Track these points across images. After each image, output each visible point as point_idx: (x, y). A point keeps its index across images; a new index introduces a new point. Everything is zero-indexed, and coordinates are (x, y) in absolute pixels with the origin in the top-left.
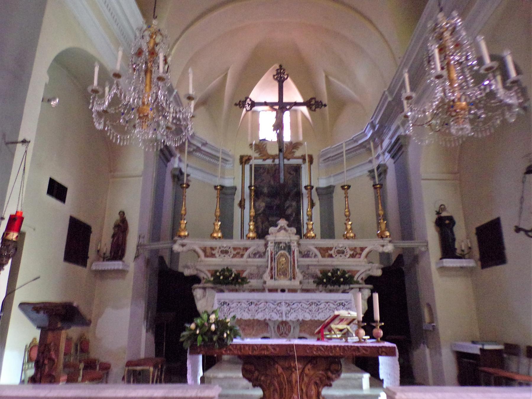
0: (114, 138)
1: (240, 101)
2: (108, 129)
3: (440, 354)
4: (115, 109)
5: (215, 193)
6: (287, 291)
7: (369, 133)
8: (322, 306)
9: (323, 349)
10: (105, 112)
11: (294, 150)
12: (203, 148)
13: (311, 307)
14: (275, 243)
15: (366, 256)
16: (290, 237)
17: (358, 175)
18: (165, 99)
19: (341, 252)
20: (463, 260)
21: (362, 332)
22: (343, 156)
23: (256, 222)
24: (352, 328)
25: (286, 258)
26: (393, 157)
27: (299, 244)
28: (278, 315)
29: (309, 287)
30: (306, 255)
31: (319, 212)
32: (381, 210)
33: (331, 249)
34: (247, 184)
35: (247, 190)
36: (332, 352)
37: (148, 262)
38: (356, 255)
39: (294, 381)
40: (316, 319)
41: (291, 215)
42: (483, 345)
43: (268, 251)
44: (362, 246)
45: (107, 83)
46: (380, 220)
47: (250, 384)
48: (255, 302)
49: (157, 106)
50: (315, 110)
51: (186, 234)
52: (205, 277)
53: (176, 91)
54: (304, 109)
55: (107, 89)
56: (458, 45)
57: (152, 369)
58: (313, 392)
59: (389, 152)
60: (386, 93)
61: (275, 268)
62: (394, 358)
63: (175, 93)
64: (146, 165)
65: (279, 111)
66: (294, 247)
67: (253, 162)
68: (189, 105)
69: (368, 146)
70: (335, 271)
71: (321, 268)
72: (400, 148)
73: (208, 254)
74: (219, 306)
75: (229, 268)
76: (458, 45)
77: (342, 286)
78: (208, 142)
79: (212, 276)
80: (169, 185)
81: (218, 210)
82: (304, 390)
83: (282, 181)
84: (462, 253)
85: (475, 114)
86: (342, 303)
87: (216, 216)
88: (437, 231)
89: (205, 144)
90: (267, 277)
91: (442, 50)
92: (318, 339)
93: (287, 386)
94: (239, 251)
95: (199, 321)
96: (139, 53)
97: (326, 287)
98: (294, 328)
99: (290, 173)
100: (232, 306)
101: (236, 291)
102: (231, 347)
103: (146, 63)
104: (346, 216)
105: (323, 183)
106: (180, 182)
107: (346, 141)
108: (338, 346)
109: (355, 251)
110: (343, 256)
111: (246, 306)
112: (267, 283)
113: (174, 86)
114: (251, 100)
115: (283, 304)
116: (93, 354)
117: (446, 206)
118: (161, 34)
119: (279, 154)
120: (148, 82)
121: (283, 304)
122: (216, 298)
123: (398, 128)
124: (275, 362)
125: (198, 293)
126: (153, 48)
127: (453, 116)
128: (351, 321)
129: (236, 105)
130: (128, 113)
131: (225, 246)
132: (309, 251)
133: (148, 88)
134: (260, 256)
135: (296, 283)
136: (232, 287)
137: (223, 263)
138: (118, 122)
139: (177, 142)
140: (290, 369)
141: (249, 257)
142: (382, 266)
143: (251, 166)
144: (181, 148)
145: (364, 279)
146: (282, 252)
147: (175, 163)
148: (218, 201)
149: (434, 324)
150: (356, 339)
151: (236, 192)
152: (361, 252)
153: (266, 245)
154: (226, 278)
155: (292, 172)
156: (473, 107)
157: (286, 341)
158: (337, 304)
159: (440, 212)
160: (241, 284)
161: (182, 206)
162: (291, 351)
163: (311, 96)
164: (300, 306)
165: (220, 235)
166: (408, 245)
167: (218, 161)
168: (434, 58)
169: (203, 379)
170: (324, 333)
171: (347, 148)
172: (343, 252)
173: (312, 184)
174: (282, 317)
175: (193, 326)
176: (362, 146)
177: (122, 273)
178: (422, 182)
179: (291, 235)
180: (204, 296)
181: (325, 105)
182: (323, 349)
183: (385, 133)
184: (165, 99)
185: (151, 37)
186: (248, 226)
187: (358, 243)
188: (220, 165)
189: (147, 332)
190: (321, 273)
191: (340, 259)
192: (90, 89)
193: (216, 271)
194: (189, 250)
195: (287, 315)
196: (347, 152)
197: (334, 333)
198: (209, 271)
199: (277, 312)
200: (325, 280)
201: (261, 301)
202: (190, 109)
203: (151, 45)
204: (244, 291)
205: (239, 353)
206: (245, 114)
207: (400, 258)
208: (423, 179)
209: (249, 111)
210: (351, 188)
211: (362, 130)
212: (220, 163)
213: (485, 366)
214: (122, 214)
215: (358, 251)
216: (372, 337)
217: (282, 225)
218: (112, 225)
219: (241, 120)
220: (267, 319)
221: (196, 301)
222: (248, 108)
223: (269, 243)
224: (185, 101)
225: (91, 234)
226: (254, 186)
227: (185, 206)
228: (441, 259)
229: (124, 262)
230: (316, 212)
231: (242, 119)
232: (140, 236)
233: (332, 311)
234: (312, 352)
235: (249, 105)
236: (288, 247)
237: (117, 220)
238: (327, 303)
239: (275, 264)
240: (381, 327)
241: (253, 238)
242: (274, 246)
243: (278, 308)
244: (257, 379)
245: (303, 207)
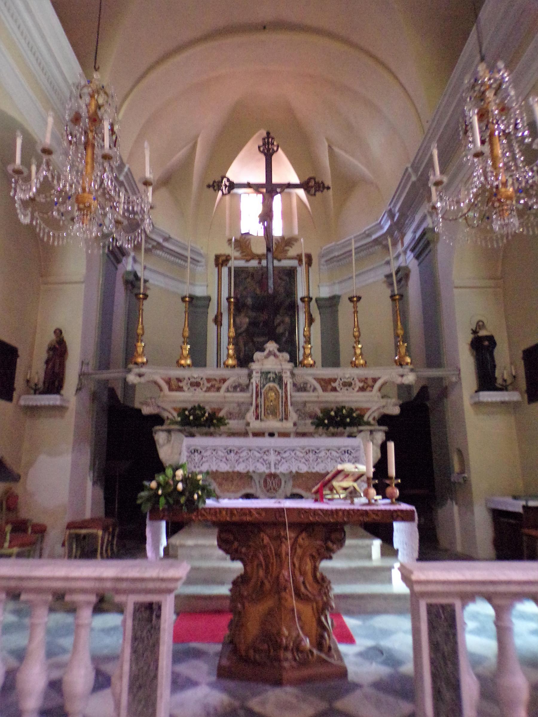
0: (46, 235)
1: (214, 182)
2: (37, 223)
3: (473, 514)
4: (46, 197)
5: (182, 307)
6: (276, 435)
7: (386, 224)
8: (322, 454)
9: (321, 514)
10: (32, 200)
11: (287, 248)
12: (166, 244)
13: (307, 456)
14: (262, 373)
15: (380, 390)
16: (281, 365)
17: (371, 281)
18: (113, 184)
19: (348, 384)
20: (505, 393)
21: (373, 491)
22: (351, 255)
23: (236, 344)
24: (360, 486)
25: (277, 393)
26: (417, 257)
27: (293, 375)
28: (265, 466)
29: (306, 430)
30: (301, 388)
32: (401, 329)
33: (335, 380)
34: (225, 294)
35: (225, 303)
36: (333, 518)
37: (94, 397)
38: (367, 387)
39: (284, 554)
40: (314, 471)
41: (283, 334)
42: (527, 501)
43: (252, 383)
44: (374, 376)
45: (34, 160)
46: (399, 341)
47: (228, 557)
48: (236, 450)
49: (104, 194)
50: (315, 195)
51: (145, 360)
52: (170, 417)
53: (127, 166)
54: (301, 192)
55: (34, 168)
56: (504, 109)
57: (100, 533)
58: (308, 567)
59: (412, 250)
61: (261, 405)
62: (412, 523)
63: (126, 170)
64: (89, 268)
65: (267, 196)
66: (287, 379)
67: (233, 263)
68: (146, 192)
69: (384, 243)
70: (339, 410)
71: (322, 405)
72: (428, 243)
73: (174, 387)
74: (188, 455)
75: (201, 405)
76: (504, 109)
77: (348, 429)
78: (172, 236)
79: (179, 415)
80: (120, 287)
81: (187, 329)
82: (297, 565)
83: (271, 291)
84: (504, 383)
85: (526, 203)
86: (348, 451)
87: (184, 337)
88: (472, 355)
89: (167, 239)
90: (251, 418)
91: (483, 115)
92: (316, 500)
93: (275, 559)
94: (214, 382)
95: (161, 478)
96: (76, 119)
97: (327, 429)
98: (285, 482)
99: (281, 279)
100: (205, 455)
101: (211, 434)
102: (203, 512)
103: (86, 133)
104: (354, 337)
105: (325, 292)
106: (136, 291)
107: (355, 235)
108: (340, 510)
109: (365, 382)
110: (350, 389)
111: (223, 455)
112: (251, 425)
113: (125, 160)
114: (228, 180)
115: (272, 452)
116: (24, 514)
117: (485, 322)
118: (105, 93)
119: (267, 254)
120: (89, 160)
121: (272, 452)
122: (184, 444)
123: (424, 218)
124: (260, 530)
125: (160, 437)
126: (96, 113)
127: (495, 208)
128: (358, 477)
129: (209, 186)
130: (64, 202)
131: (195, 376)
132: (306, 384)
133: (89, 167)
134: (242, 390)
135: (288, 425)
136: (205, 430)
137: (192, 399)
138: (50, 214)
139: (130, 242)
140: (279, 539)
141: (228, 390)
142: (401, 402)
143: (230, 269)
144: (137, 248)
146: (271, 384)
147: (128, 265)
148: (187, 317)
149: (466, 475)
150: (364, 500)
151: (211, 303)
152: (372, 384)
153: (250, 376)
154: (197, 418)
156: (523, 195)
157: (275, 503)
158: (341, 452)
159: (478, 330)
160: (217, 426)
161: (139, 323)
162: (280, 517)
163: (312, 175)
164: (293, 454)
165: (189, 362)
167: (186, 261)
168: (472, 128)
169: (166, 550)
170: (324, 492)
171: (359, 244)
172: (350, 384)
173: (311, 295)
174: (270, 468)
175: (153, 484)
176: (376, 241)
177: (61, 409)
178: (455, 291)
179: (283, 363)
180: (169, 441)
181: (328, 188)
182: (321, 514)
183: (407, 224)
184: (113, 184)
185: (92, 96)
186: (226, 350)
187: (369, 373)
188: (189, 267)
189: (93, 485)
190: (322, 412)
192: (10, 168)
193: (185, 409)
194: (148, 382)
195: (277, 466)
196: (356, 250)
197: (337, 492)
198: (175, 409)
199: (263, 462)
200: (326, 421)
201: (244, 448)
202: (148, 198)
203: (93, 107)
204: (220, 435)
205: (214, 519)
206: (221, 199)
207: (424, 390)
208: (456, 287)
209: (226, 194)
210: (362, 300)
211: (377, 220)
212: (189, 264)
213: (528, 528)
214: (59, 332)
215: (370, 382)
216: (384, 497)
217: (271, 349)
218: (45, 347)
220: (251, 470)
221: (158, 447)
222: (225, 191)
223: (254, 373)
224: (141, 187)
225: (18, 360)
226: (234, 298)
227: (142, 324)
228: (476, 392)
229: (62, 395)
230: (316, 329)
231: (218, 205)
232: (83, 362)
233: (334, 461)
234: (308, 518)
235: (226, 186)
236: (279, 379)
237: (53, 341)
238: (329, 450)
239: (261, 401)
240: (397, 485)
241: (233, 367)
242: (261, 377)
243: (265, 457)
244: (236, 551)
245: (298, 321)
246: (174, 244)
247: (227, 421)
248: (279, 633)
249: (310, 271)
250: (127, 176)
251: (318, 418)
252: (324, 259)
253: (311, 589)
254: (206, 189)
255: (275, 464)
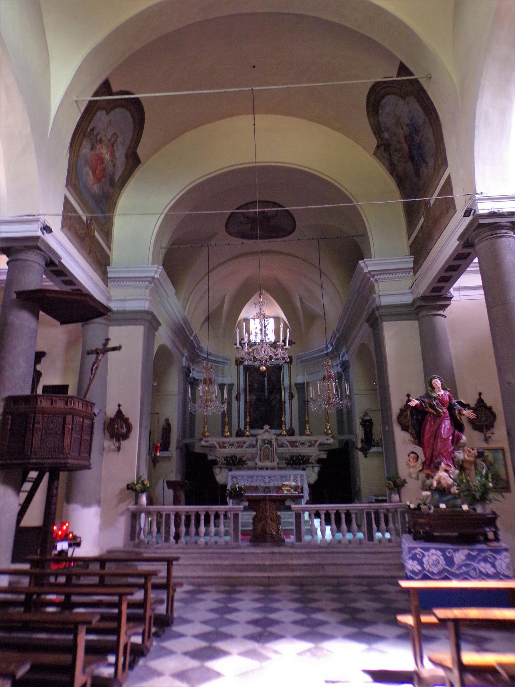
19: (303, 444)
27: (276, 440)
31: (297, 404)
33: (296, 442)
53: (195, 332)
60: (336, 331)
63: (194, 334)
66: (274, 443)
70: (298, 457)
71: (290, 454)
79: (225, 460)
105: (300, 380)
110: (304, 446)
125: (217, 470)
132: (283, 443)
134: (253, 447)
135: (275, 464)
140: (266, 504)
145: (316, 460)
146: (266, 445)
153: (257, 440)
154: (234, 462)
155: (276, 371)
160: (242, 465)
166: (219, 508)
177: (169, 458)
180: (220, 472)
187: (313, 438)
191: (302, 448)
208: (355, 395)
214: (167, 420)
219: (237, 324)
226: (249, 403)
230: (295, 401)
236: (270, 443)
243: (264, 480)
246: (213, 356)
247: (247, 462)
248: (266, 529)
249: (291, 366)
250: (194, 337)
251: (288, 460)
252: (299, 361)
253: (275, 518)
254: (296, 342)
255: (268, 483)
